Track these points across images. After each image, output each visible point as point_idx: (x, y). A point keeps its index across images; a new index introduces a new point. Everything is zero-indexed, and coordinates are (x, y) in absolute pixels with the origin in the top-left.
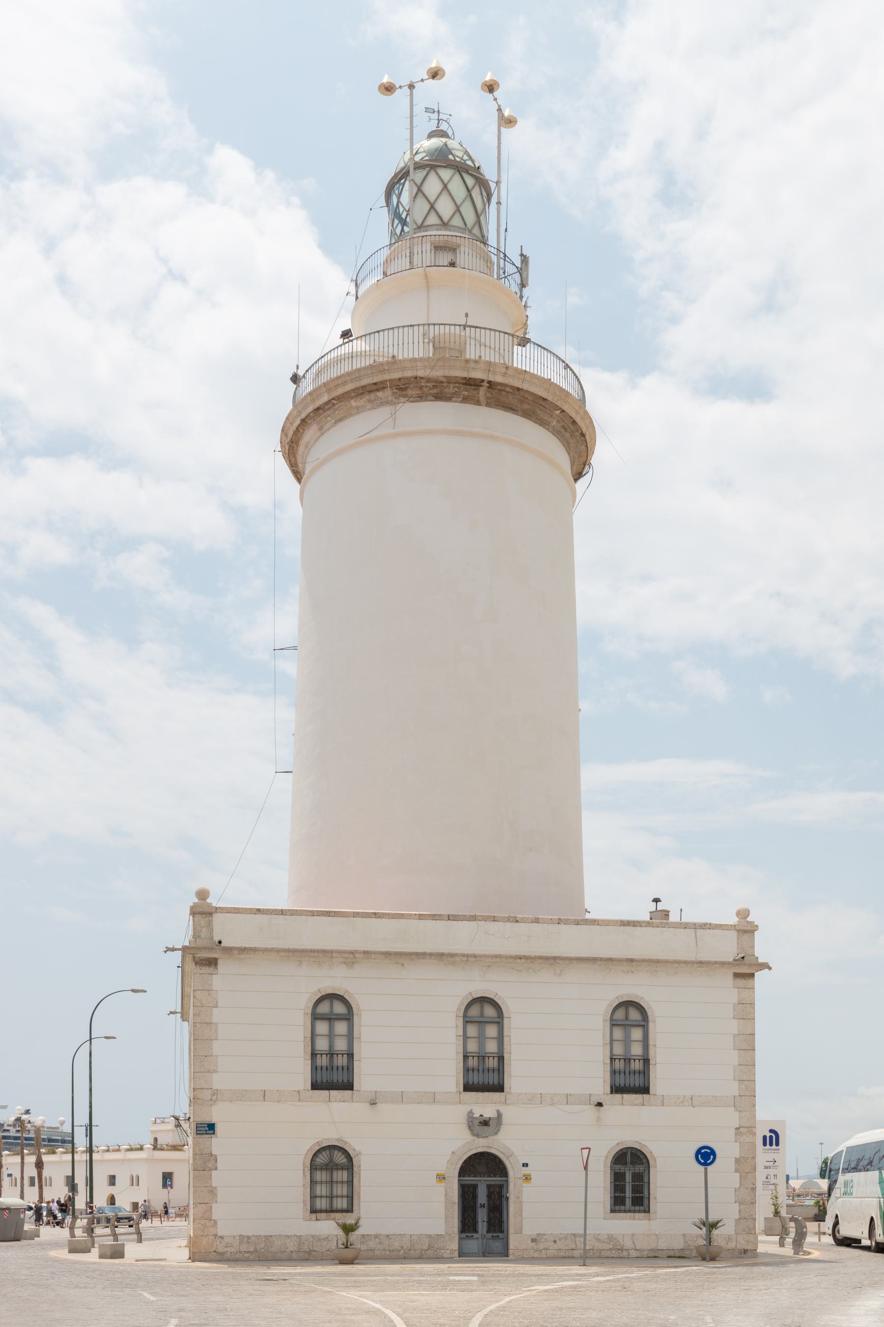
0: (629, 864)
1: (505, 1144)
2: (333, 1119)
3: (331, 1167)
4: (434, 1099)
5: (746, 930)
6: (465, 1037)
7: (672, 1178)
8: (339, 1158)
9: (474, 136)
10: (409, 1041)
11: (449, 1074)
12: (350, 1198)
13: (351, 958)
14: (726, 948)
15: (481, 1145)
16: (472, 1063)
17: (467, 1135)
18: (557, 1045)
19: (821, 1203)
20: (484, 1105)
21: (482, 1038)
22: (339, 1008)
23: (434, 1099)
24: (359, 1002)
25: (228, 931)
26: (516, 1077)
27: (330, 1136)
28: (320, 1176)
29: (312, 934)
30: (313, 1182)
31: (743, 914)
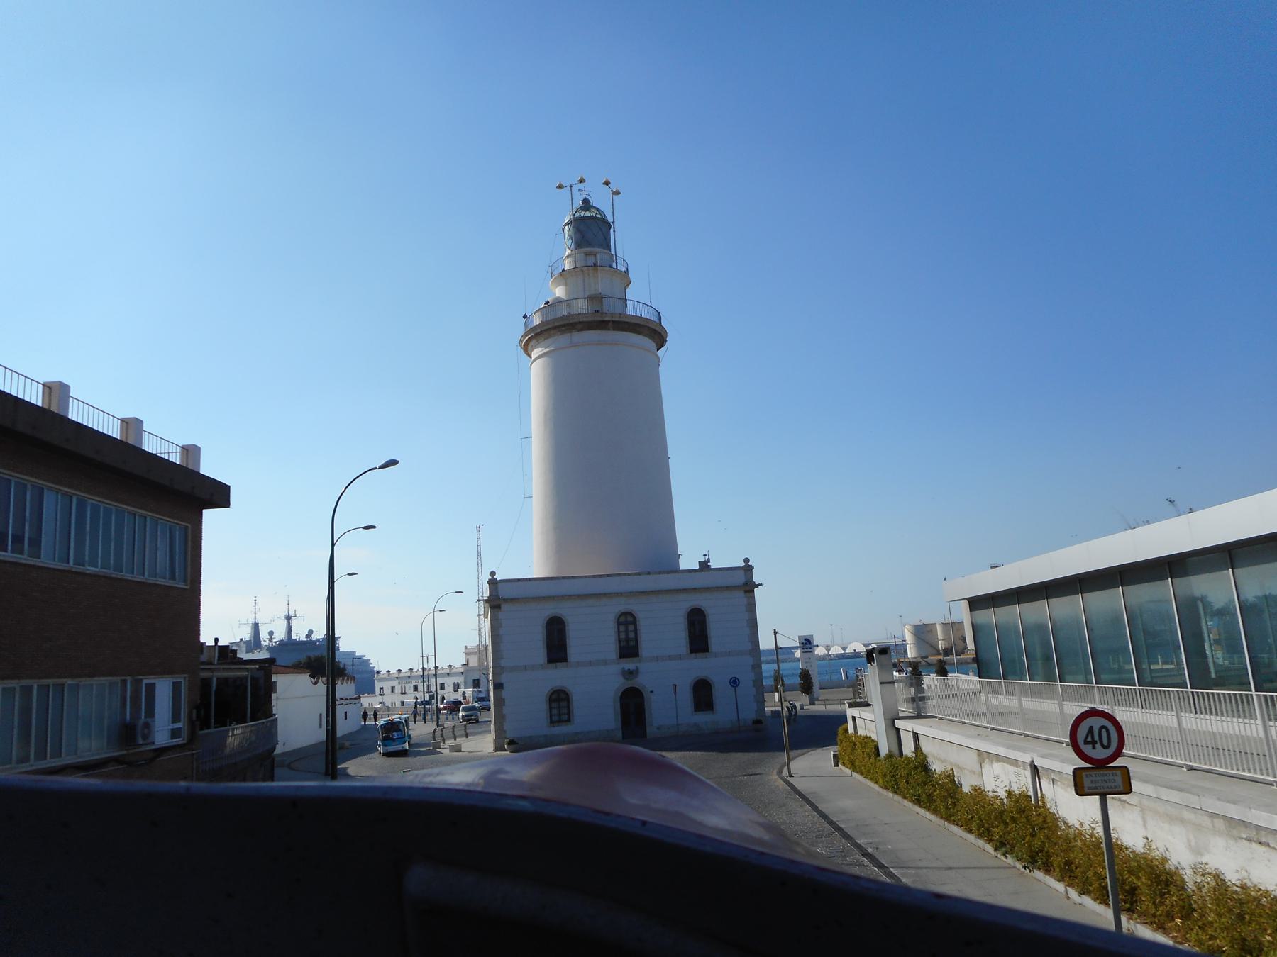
0: (700, 541)
1: (643, 681)
2: (558, 677)
3: (558, 700)
4: (605, 663)
5: (748, 569)
6: (619, 632)
7: (721, 693)
8: (563, 696)
9: (601, 201)
10: (592, 635)
11: (610, 648)
12: (569, 714)
13: (630, 594)
14: (740, 579)
15: (630, 684)
16: (623, 644)
17: (622, 680)
18: (663, 632)
19: (395, 735)
20: (630, 665)
21: (627, 631)
22: (630, 619)
23: (605, 663)
24: (641, 616)
25: (504, 592)
26: (646, 648)
27: (558, 684)
28: (554, 705)
29: (615, 585)
30: (551, 708)
31: (747, 560)
